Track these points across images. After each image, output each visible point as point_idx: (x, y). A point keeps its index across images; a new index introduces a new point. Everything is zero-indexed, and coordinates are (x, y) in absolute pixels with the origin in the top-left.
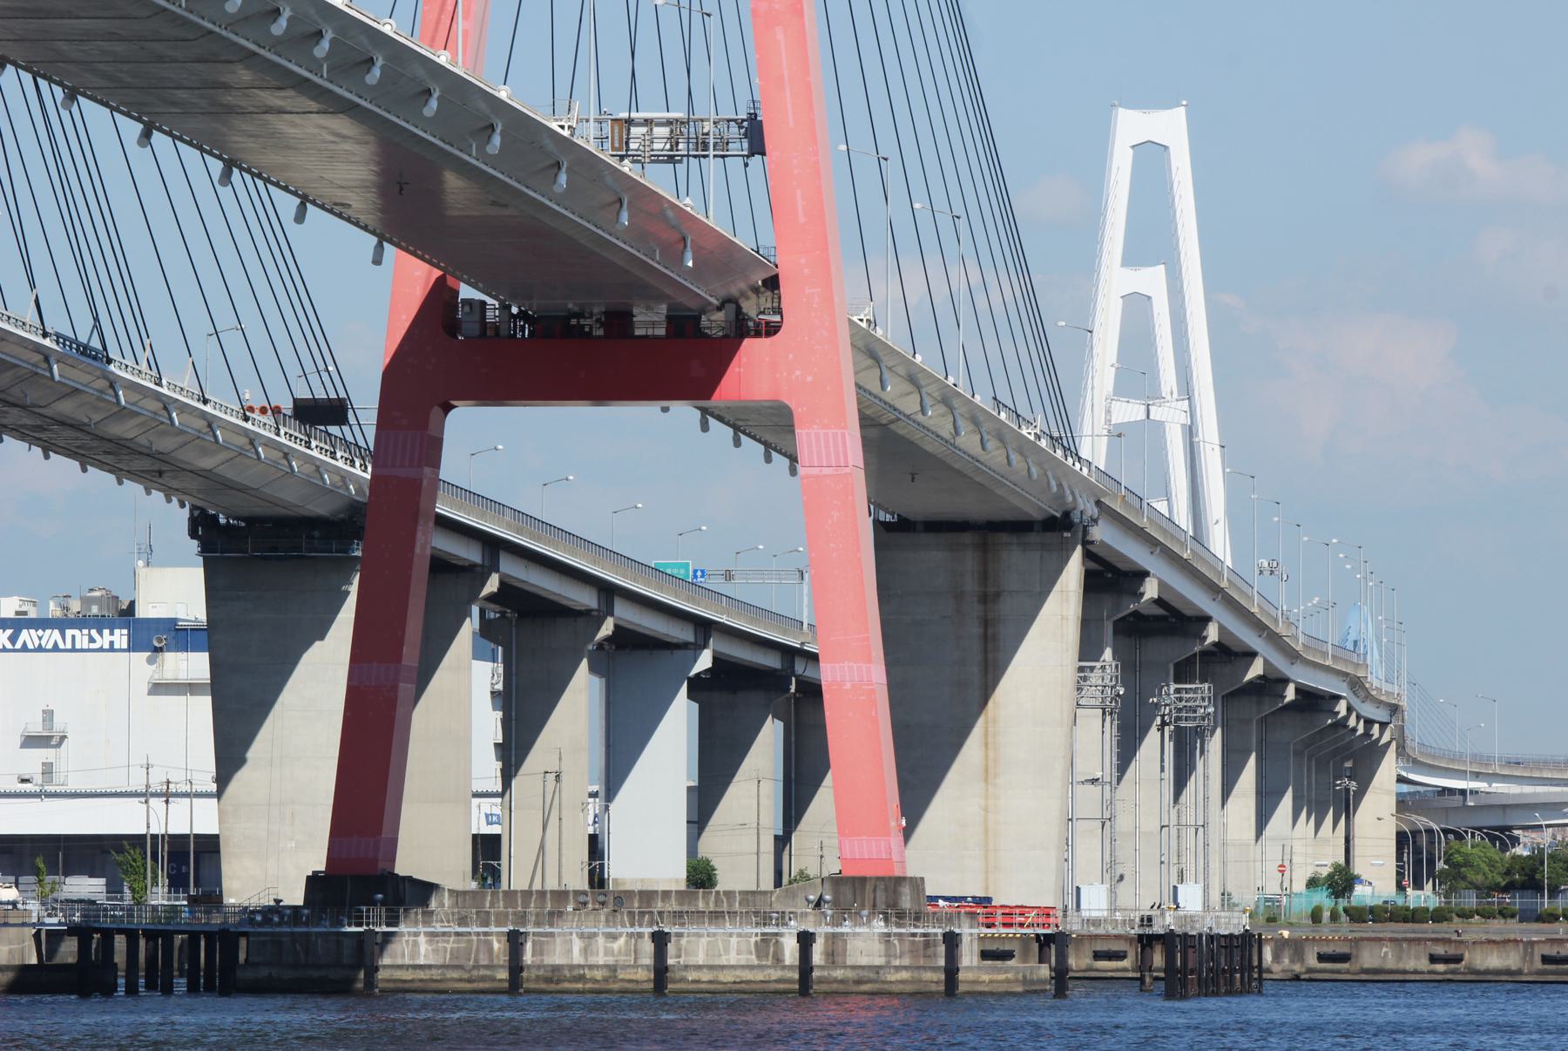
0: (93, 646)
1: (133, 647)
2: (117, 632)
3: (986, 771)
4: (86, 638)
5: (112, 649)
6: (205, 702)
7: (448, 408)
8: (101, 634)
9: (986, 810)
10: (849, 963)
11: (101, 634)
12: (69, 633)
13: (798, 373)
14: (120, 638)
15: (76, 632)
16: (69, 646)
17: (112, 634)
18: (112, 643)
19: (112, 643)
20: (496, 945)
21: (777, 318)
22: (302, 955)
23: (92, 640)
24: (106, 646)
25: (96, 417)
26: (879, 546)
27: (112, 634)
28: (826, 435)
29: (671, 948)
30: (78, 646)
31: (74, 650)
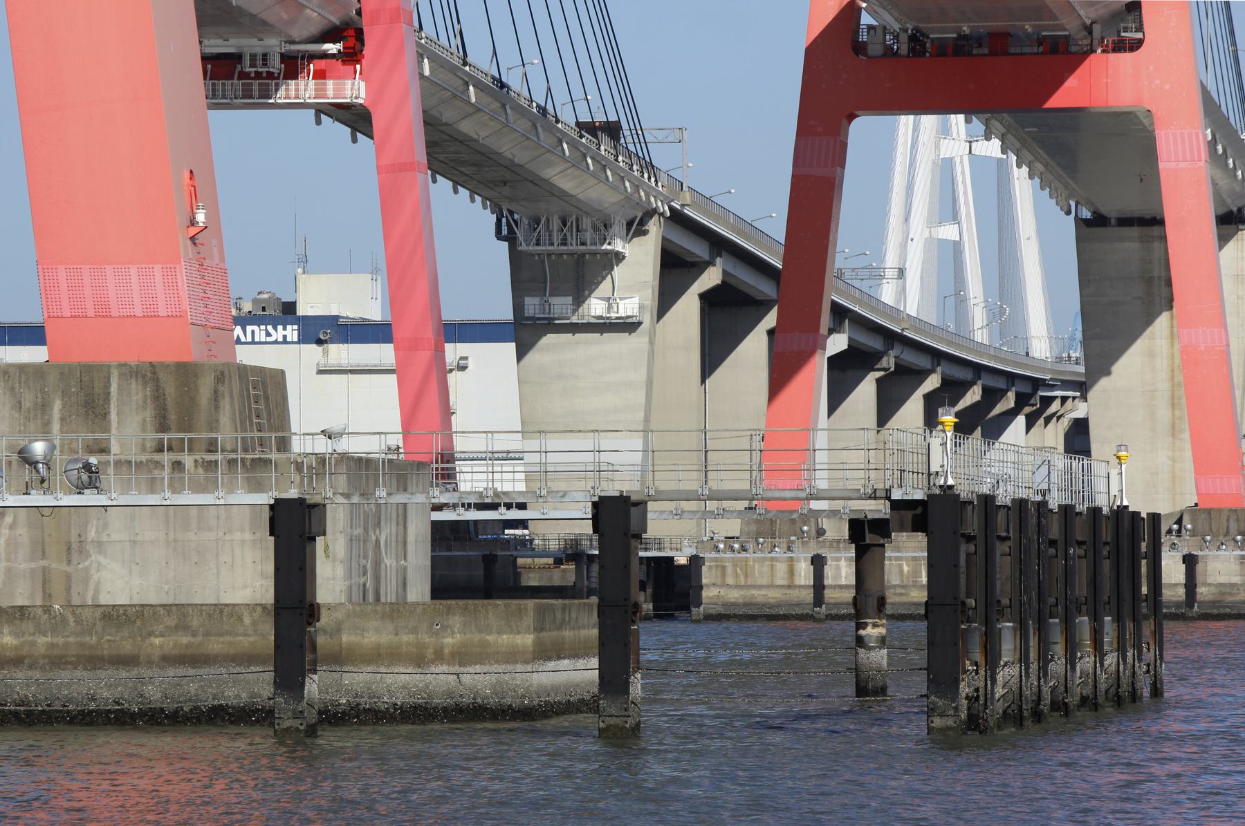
0: (269, 339)
1: (303, 340)
2: (289, 327)
3: (1173, 427)
4: (263, 333)
5: (285, 341)
6: (393, 378)
7: (851, 117)
8: (276, 329)
9: (1174, 460)
10: (1209, 581)
11: (276, 329)
12: (249, 329)
13: (1157, 82)
14: (292, 332)
15: (255, 328)
16: (249, 339)
17: (285, 329)
18: (285, 337)
19: (285, 337)
20: (906, 569)
21: (1140, 35)
22: (742, 578)
23: (268, 334)
24: (280, 339)
25: (483, 134)
26: (1079, 239)
27: (285, 329)
28: (1182, 134)
29: (1199, 567)
30: (257, 339)
31: (253, 342)
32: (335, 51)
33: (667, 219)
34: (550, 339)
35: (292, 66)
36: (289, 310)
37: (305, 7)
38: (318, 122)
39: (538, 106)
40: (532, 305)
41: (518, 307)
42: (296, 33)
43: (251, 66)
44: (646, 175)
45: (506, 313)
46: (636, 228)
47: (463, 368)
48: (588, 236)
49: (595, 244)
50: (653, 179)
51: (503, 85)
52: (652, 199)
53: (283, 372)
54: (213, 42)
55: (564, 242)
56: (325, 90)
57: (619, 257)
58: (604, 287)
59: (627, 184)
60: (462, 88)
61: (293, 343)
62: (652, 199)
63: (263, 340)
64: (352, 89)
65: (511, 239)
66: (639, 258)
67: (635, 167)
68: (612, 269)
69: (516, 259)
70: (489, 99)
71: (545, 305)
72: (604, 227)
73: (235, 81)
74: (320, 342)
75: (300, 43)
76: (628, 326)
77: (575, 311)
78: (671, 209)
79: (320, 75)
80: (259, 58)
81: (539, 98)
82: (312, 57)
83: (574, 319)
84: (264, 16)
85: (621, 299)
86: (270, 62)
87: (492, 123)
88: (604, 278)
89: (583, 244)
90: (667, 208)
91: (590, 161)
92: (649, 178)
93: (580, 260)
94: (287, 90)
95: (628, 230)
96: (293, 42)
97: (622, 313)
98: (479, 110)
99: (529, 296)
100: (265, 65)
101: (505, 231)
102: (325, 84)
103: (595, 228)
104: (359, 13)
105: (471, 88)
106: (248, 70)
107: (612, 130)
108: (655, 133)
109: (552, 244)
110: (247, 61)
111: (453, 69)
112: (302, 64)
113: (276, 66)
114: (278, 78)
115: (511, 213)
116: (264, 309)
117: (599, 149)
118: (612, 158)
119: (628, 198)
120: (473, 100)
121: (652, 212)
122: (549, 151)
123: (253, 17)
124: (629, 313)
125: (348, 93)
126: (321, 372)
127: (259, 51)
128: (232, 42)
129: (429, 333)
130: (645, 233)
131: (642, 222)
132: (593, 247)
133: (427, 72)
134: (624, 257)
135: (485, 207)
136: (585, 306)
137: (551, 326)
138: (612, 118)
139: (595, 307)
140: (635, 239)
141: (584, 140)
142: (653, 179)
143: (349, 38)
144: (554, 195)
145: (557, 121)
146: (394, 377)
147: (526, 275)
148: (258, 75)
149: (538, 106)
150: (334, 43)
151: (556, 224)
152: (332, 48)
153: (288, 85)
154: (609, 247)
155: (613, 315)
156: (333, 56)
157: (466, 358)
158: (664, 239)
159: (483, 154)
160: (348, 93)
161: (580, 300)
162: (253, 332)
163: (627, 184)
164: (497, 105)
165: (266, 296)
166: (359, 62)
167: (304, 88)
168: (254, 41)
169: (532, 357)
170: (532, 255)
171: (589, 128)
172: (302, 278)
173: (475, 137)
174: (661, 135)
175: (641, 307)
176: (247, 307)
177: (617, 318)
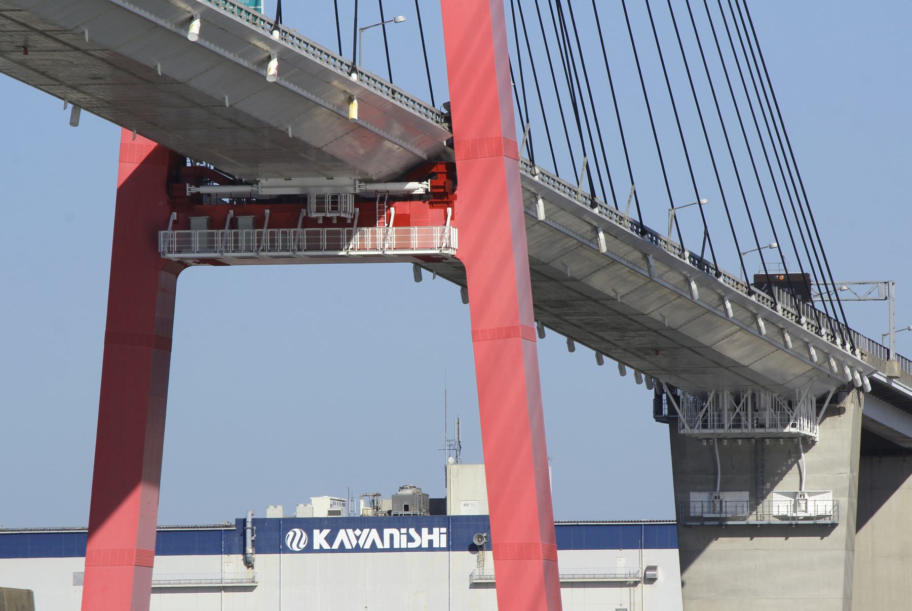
0: (411, 545)
2: (436, 530)
4: (404, 538)
5: (431, 548)
8: (420, 533)
12: (387, 532)
14: (439, 536)
15: (394, 531)
16: (387, 546)
17: (431, 532)
18: (431, 542)
19: (431, 542)
23: (410, 539)
24: (425, 545)
25: (622, 291)
27: (431, 532)
30: (396, 546)
31: (392, 549)
32: (421, 191)
33: (866, 394)
34: (720, 545)
35: (369, 210)
36: (438, 507)
37: (383, 138)
38: (418, 278)
39: (692, 255)
40: (699, 501)
41: (682, 505)
42: (373, 170)
43: (318, 211)
44: (839, 341)
45: (664, 510)
46: (828, 405)
47: (651, 580)
48: (767, 415)
49: (776, 426)
50: (848, 346)
51: (644, 231)
52: (848, 371)
53: (29, 594)
54: (272, 181)
55: (737, 424)
56: (409, 239)
57: (808, 443)
58: (789, 481)
59: (813, 352)
60: (590, 235)
61: (440, 549)
62: (848, 371)
63: (404, 546)
64: (444, 238)
65: (672, 420)
66: (834, 442)
67: (823, 331)
68: (800, 457)
69: (678, 444)
70: (627, 248)
71: (715, 502)
72: (787, 405)
73: (299, 229)
74: (474, 548)
75: (378, 181)
76: (819, 528)
77: (753, 507)
78: (873, 382)
79: (402, 221)
80: (328, 200)
81: (694, 245)
82: (394, 198)
83: (752, 520)
84: (330, 149)
85: (810, 494)
86: (341, 206)
87: (632, 278)
88: (789, 468)
89: (762, 426)
90: (867, 381)
91: (761, 323)
92: (843, 345)
93: (759, 446)
94: (362, 239)
95: (819, 409)
96: (370, 181)
97: (811, 512)
98: (614, 262)
99: (695, 491)
100: (335, 209)
101: (665, 412)
102: (409, 232)
103: (776, 406)
104: (451, 144)
105: (601, 235)
106: (314, 215)
107: (798, 286)
108: (855, 288)
109: (723, 427)
110: (313, 204)
111: (578, 212)
112: (381, 208)
113: (349, 210)
114: (351, 225)
115: (672, 389)
116: (406, 508)
117: (775, 308)
118: (792, 320)
119: (817, 368)
120: (604, 249)
121: (851, 386)
122: (709, 311)
123: (319, 150)
124: (821, 512)
125: (437, 242)
126: (475, 585)
127: (328, 192)
128: (296, 181)
129: (541, 541)
130: (840, 411)
131: (837, 399)
132: (774, 430)
133: (542, 216)
134: (814, 442)
135: (639, 381)
136: (766, 502)
137: (722, 528)
138: (794, 270)
139: (778, 505)
140: (828, 419)
141: (753, 298)
142: (848, 346)
143: (438, 173)
144: (720, 366)
145: (718, 274)
146: (493, 592)
147: (692, 466)
148: (327, 222)
149: (692, 255)
150: (420, 181)
151: (727, 401)
152: (418, 187)
153: (363, 233)
154: (793, 430)
155: (801, 514)
156: (420, 197)
157: (654, 568)
158: (865, 418)
159: (625, 316)
160: (437, 242)
161: (758, 495)
162: (392, 536)
163: (813, 352)
164: (636, 255)
165: (409, 492)
166: (450, 204)
167: (382, 237)
168: (322, 180)
169: (699, 566)
170: (698, 440)
171: (765, 282)
172: (453, 469)
173: (612, 294)
174: (862, 291)
175: (836, 506)
176: (386, 505)
177: (806, 518)
